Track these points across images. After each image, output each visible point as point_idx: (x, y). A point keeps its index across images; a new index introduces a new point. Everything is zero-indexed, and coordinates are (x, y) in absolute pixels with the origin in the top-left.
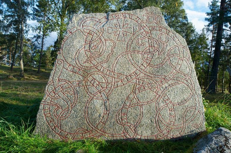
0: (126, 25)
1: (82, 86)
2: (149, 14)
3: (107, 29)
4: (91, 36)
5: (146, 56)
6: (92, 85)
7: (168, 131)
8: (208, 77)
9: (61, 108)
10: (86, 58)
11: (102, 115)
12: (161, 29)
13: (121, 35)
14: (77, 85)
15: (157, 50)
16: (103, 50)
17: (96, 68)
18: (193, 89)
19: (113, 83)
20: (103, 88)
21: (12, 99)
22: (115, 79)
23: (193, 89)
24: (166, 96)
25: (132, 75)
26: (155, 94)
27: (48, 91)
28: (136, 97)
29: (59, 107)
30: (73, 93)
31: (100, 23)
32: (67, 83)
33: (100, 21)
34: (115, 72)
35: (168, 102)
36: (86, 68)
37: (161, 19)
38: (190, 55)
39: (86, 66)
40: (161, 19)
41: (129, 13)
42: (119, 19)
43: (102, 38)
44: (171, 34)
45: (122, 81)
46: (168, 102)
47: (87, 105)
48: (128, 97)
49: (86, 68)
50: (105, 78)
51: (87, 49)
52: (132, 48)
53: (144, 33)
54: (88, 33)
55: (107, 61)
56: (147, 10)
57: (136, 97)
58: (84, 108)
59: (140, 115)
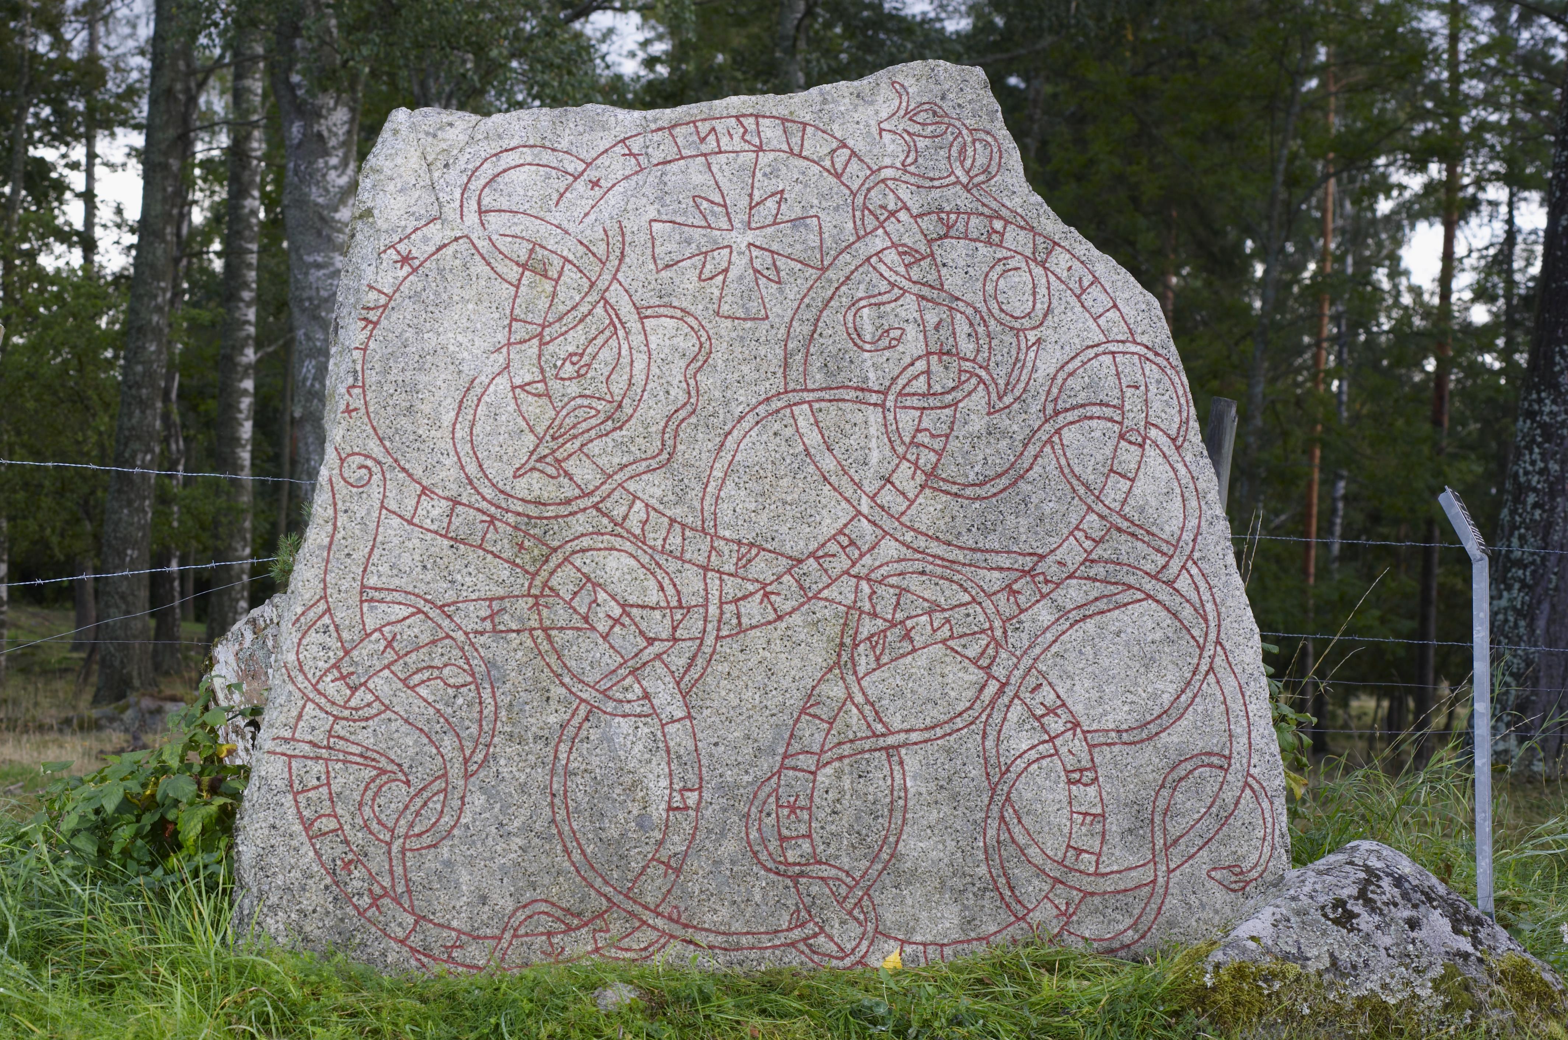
0: (771, 204)
1: (518, 632)
2: (918, 119)
3: (643, 237)
4: (548, 286)
5: (907, 420)
6: (581, 624)
7: (1063, 908)
8: (1427, 553)
9: (400, 776)
10: (530, 440)
11: (658, 811)
12: (998, 225)
13: (741, 278)
14: (488, 625)
15: (981, 380)
16: (630, 384)
17: (595, 506)
18: (1212, 636)
19: (713, 610)
20: (651, 641)
21: (1288, 534)
22: (721, 579)
23: (1212, 636)
24: (1046, 688)
25: (826, 555)
26: (976, 675)
27: (306, 668)
28: (859, 698)
29: (383, 772)
30: (469, 679)
31: (598, 192)
32: (421, 616)
33: (592, 174)
34: (721, 532)
35: (1055, 725)
36: (533, 511)
37: (996, 156)
38: (1193, 410)
39: (537, 493)
40: (996, 156)
41: (783, 112)
42: (722, 158)
43: (615, 294)
44: (1060, 261)
45: (766, 595)
46: (1055, 725)
47: (563, 756)
48: (811, 699)
49: (533, 511)
50: (660, 574)
51: (667, 621)
52: (816, 362)
53: (891, 256)
54: (524, 266)
55: (665, 456)
56: (902, 91)
57: (859, 698)
58: (540, 774)
59: (891, 811)
